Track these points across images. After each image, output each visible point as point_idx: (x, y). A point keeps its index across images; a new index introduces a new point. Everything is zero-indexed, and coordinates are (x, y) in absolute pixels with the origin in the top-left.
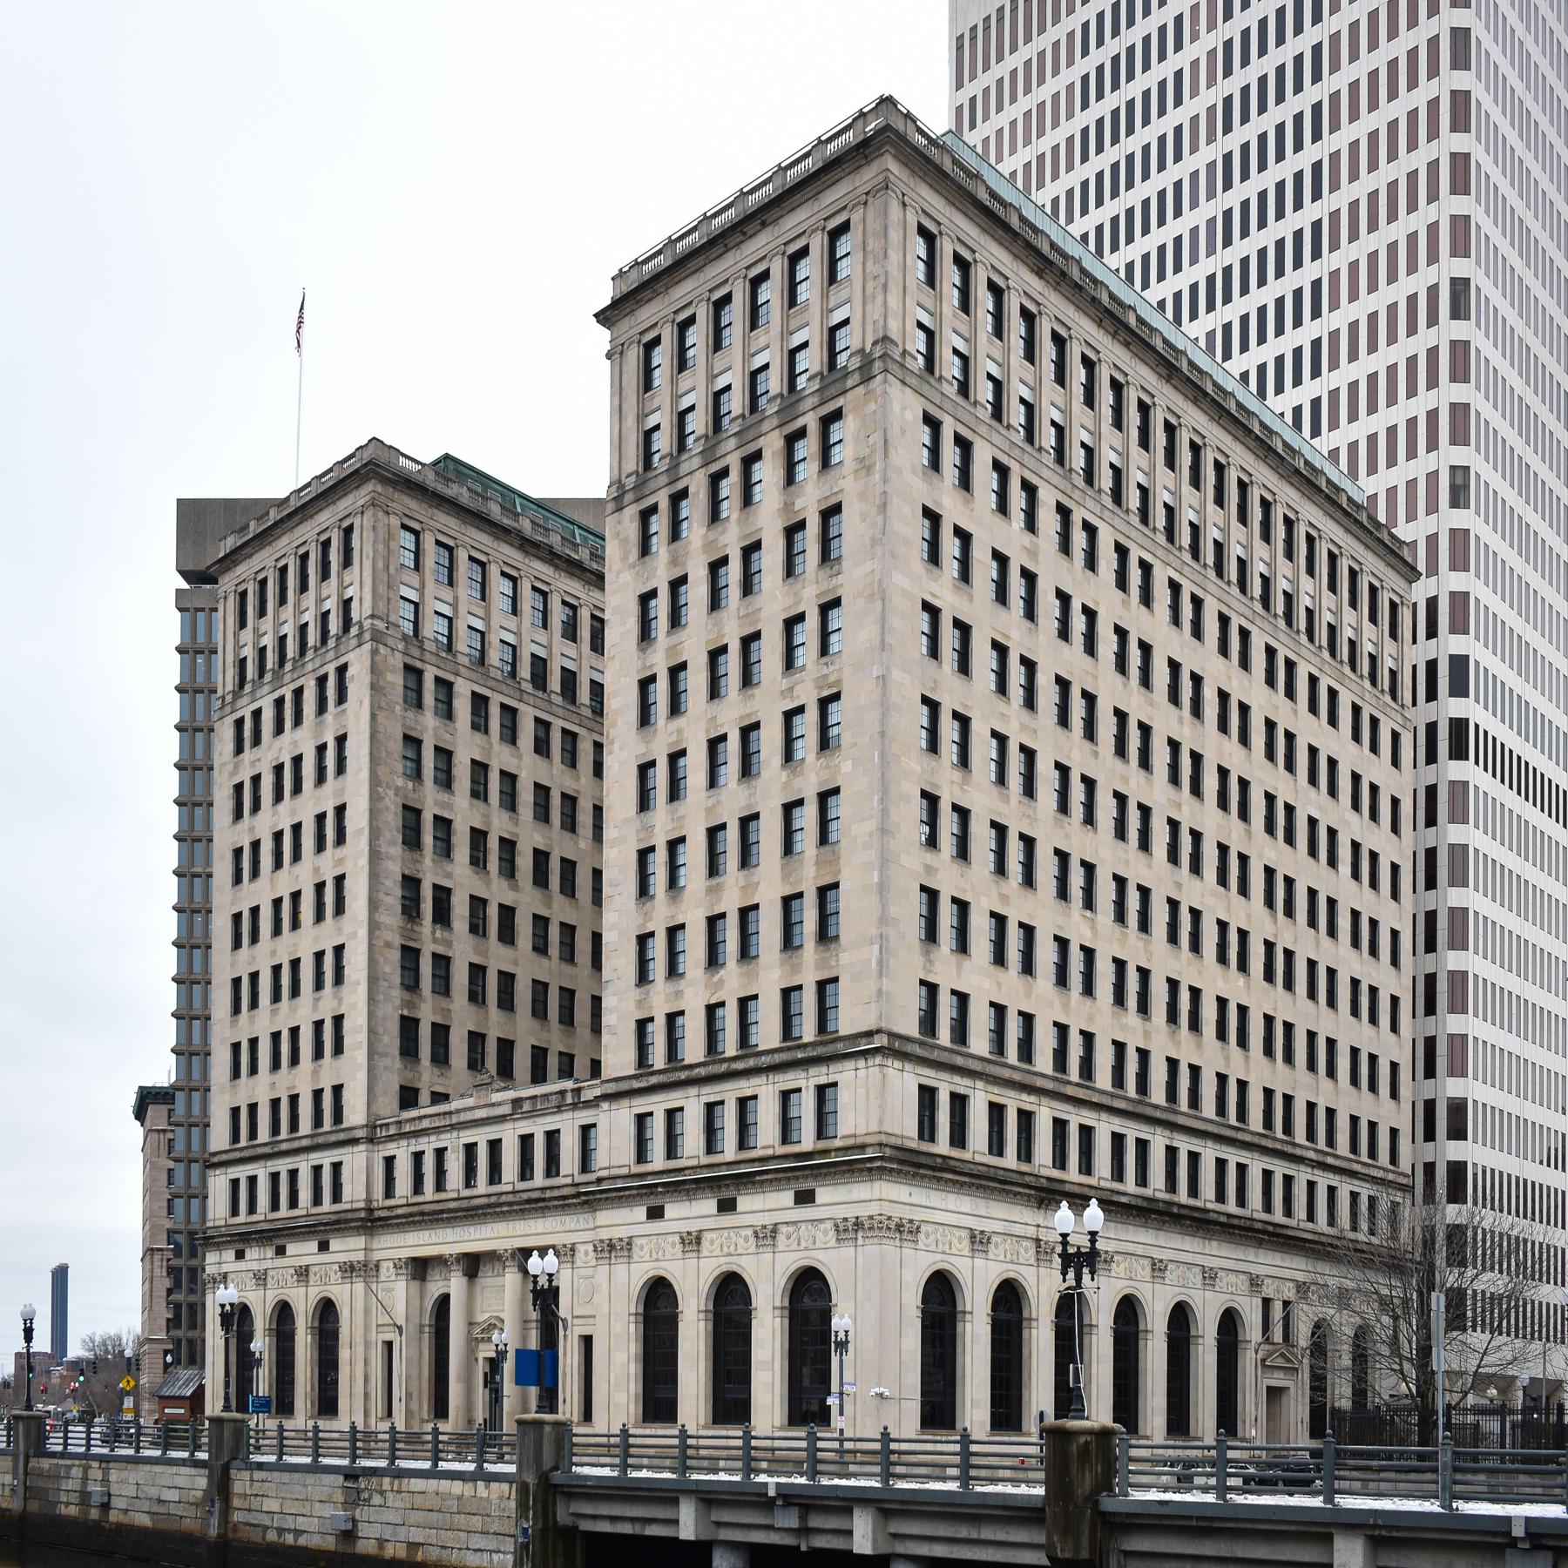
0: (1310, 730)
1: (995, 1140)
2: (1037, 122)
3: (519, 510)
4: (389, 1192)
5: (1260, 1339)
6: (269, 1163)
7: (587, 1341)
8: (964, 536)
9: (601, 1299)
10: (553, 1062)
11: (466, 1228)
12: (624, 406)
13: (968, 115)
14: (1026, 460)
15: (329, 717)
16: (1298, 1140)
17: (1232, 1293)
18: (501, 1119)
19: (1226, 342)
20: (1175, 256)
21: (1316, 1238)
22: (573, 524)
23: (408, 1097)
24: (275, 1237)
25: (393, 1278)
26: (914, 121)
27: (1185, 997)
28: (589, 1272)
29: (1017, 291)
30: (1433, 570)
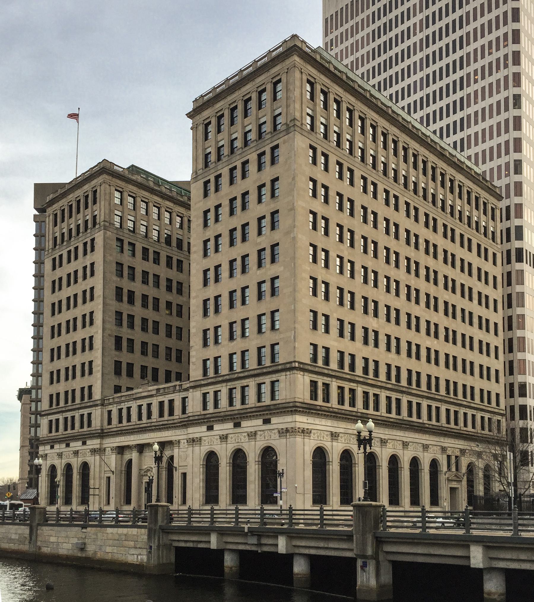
0: (461, 253)
1: (340, 400)
2: (355, 47)
3: (160, 184)
4: (110, 423)
5: (446, 470)
6: (64, 414)
7: (184, 475)
8: (351, 202)
9: (190, 460)
10: (173, 376)
11: (138, 435)
12: (198, 146)
13: (329, 45)
14: (323, 145)
15: (88, 256)
16: (459, 398)
17: (435, 453)
18: (151, 396)
19: (427, 121)
20: (409, 91)
21: (467, 433)
22: (181, 188)
23: (118, 389)
24: (67, 441)
25: (111, 454)
26: (305, 43)
27: (414, 348)
28: (185, 450)
29: (345, 102)
30: (508, 196)
